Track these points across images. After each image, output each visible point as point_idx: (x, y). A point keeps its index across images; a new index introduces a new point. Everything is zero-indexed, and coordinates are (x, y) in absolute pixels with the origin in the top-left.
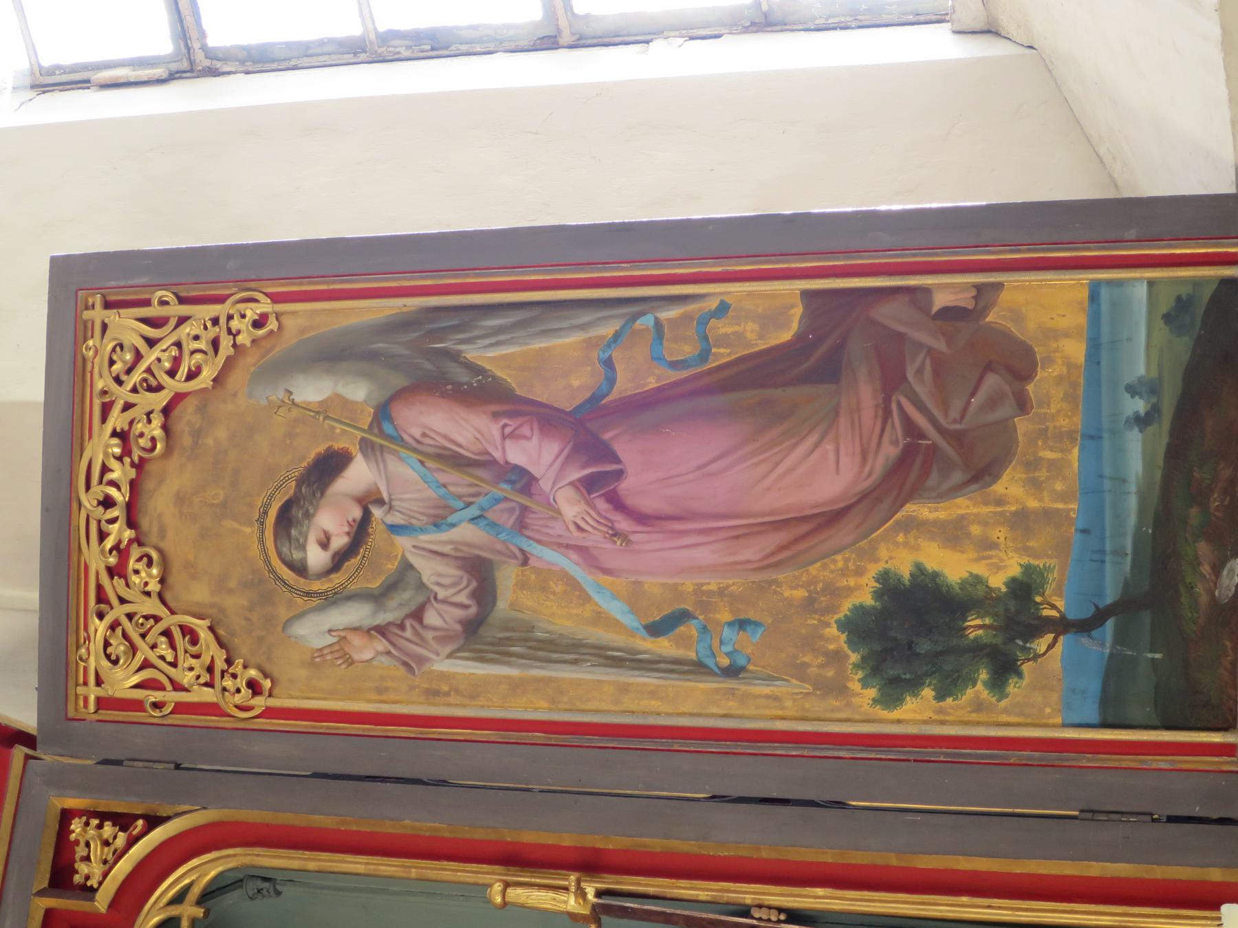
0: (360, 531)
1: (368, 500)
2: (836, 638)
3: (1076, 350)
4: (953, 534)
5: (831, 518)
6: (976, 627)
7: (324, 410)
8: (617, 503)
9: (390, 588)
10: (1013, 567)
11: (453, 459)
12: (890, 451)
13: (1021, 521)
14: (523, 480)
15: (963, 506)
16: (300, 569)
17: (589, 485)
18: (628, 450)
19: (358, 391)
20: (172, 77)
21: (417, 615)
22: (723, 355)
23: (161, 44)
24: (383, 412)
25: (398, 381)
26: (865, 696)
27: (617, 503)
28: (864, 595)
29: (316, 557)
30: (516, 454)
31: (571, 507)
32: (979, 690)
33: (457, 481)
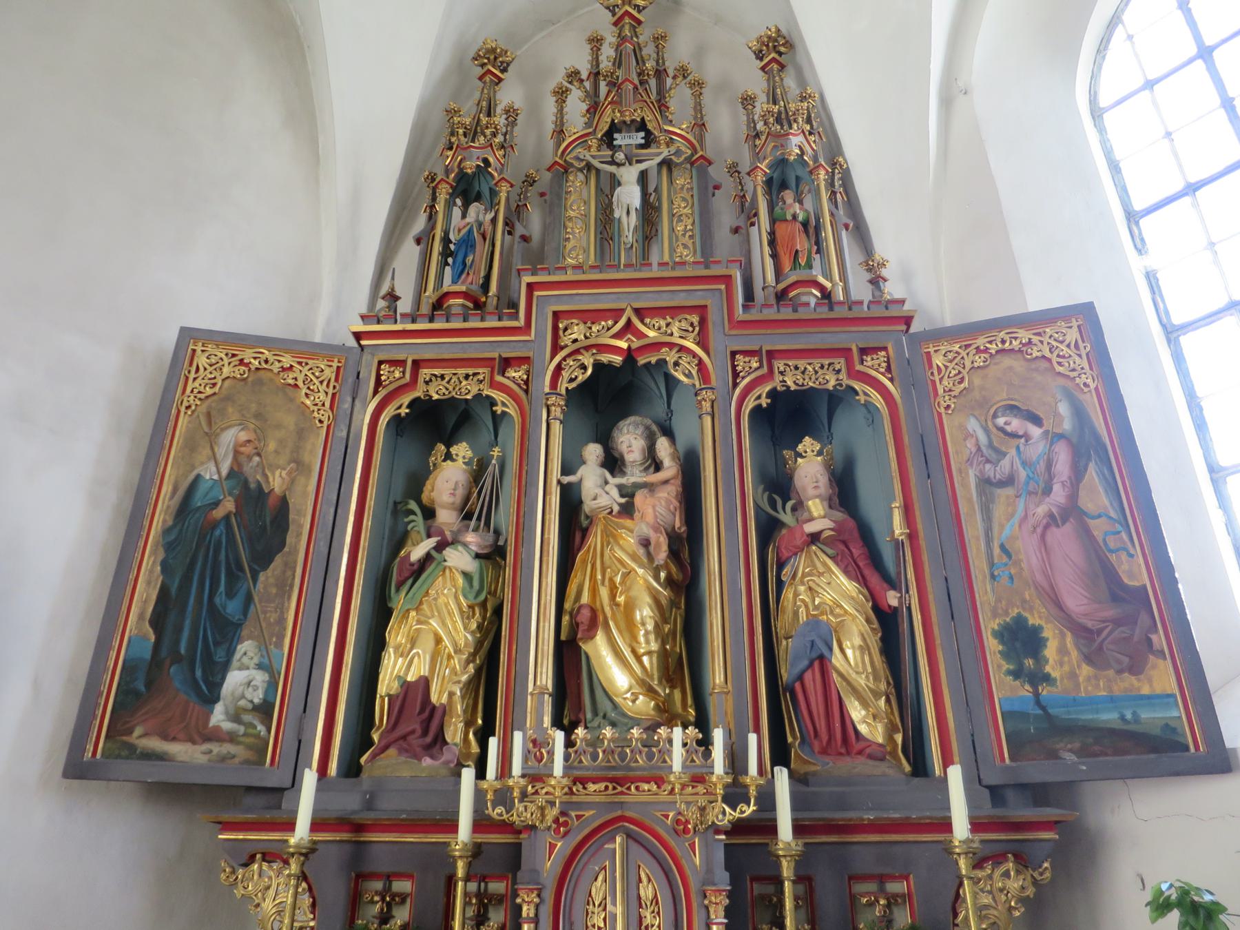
0: (1014, 435)
1: (1026, 436)
2: (1014, 612)
3: (1146, 690)
4: (1062, 651)
5: (1058, 604)
6: (1029, 663)
7: (1056, 414)
8: (1047, 527)
9: (996, 450)
10: (1055, 674)
11: (1049, 465)
12: (1089, 624)
13: (1073, 676)
14: (1048, 491)
15: (1074, 654)
16: (995, 416)
17: (1051, 516)
18: (1068, 528)
19: (1067, 426)
20: (1164, 326)
21: (988, 461)
22: (1113, 558)
23: (1177, 320)
24: (1061, 436)
25: (1075, 440)
26: (995, 625)
27: (1047, 527)
28: (1033, 620)
29: (1001, 421)
30: (1057, 488)
31: (1041, 510)
32: (1006, 666)
33: (1042, 467)
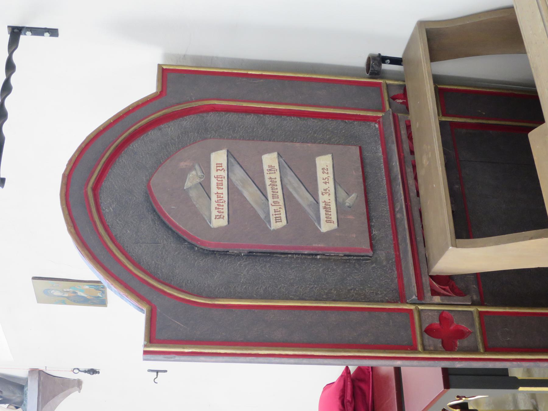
23: (159, 373)
